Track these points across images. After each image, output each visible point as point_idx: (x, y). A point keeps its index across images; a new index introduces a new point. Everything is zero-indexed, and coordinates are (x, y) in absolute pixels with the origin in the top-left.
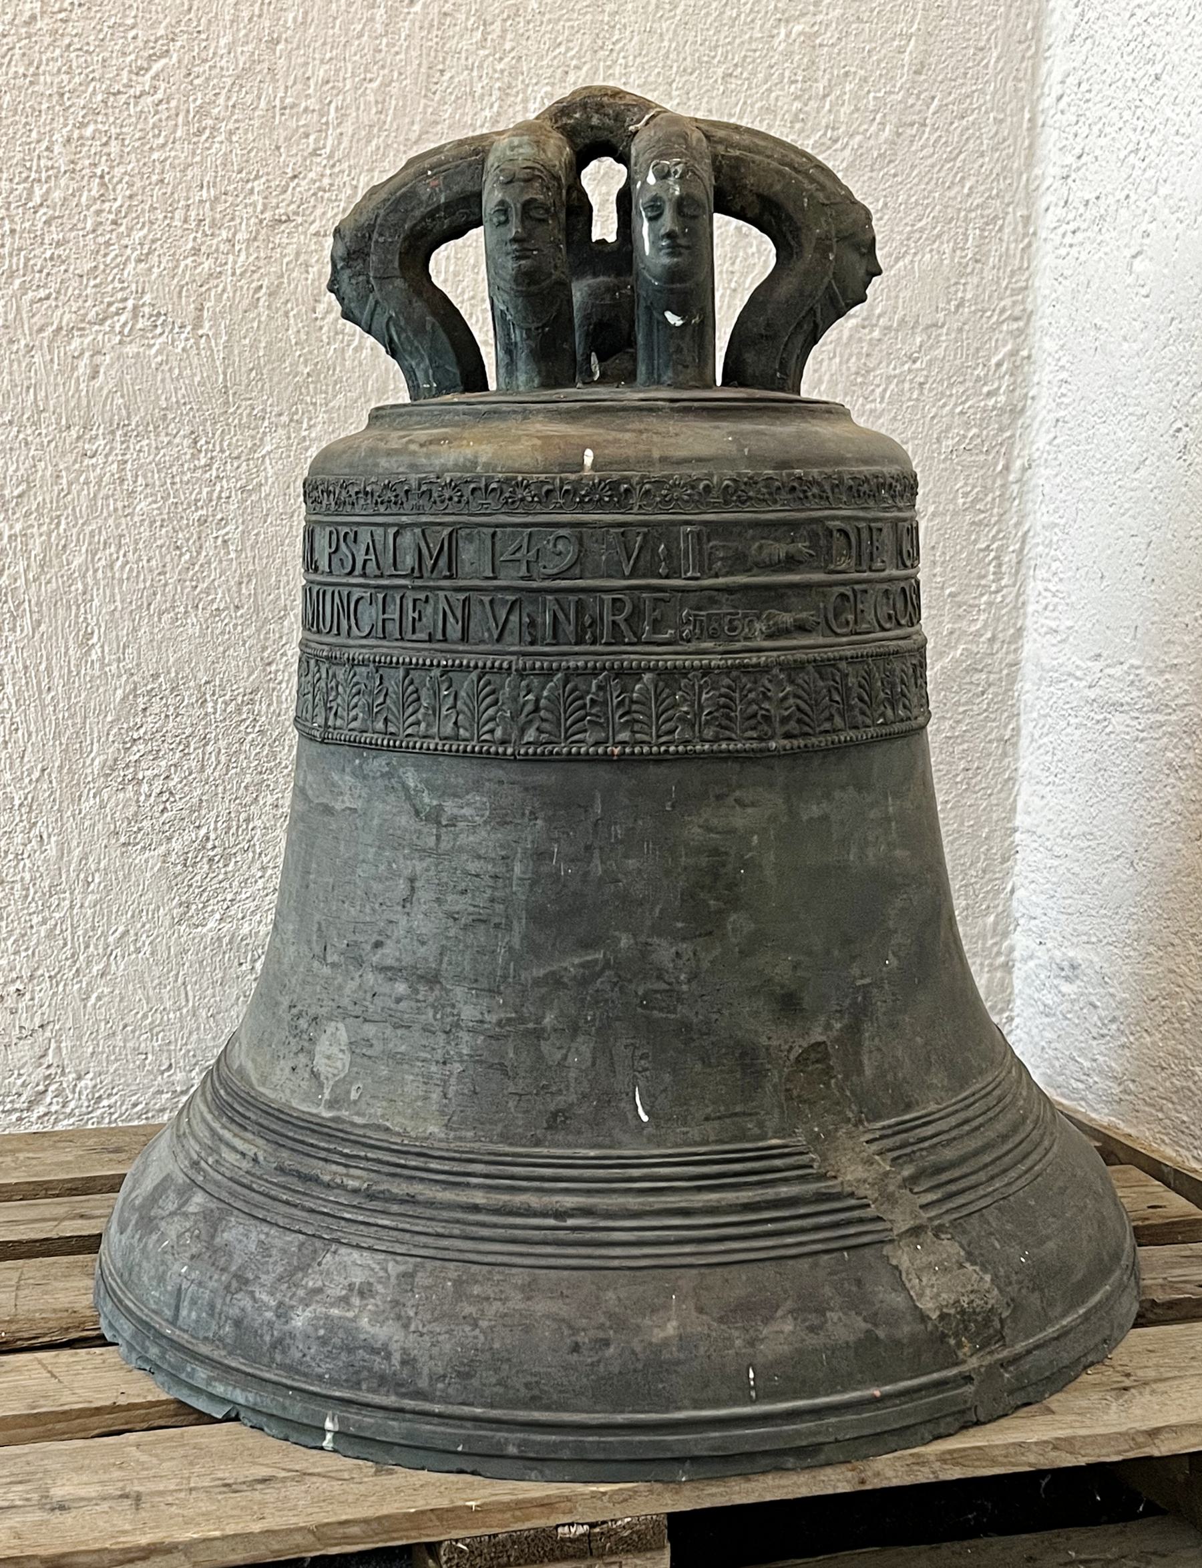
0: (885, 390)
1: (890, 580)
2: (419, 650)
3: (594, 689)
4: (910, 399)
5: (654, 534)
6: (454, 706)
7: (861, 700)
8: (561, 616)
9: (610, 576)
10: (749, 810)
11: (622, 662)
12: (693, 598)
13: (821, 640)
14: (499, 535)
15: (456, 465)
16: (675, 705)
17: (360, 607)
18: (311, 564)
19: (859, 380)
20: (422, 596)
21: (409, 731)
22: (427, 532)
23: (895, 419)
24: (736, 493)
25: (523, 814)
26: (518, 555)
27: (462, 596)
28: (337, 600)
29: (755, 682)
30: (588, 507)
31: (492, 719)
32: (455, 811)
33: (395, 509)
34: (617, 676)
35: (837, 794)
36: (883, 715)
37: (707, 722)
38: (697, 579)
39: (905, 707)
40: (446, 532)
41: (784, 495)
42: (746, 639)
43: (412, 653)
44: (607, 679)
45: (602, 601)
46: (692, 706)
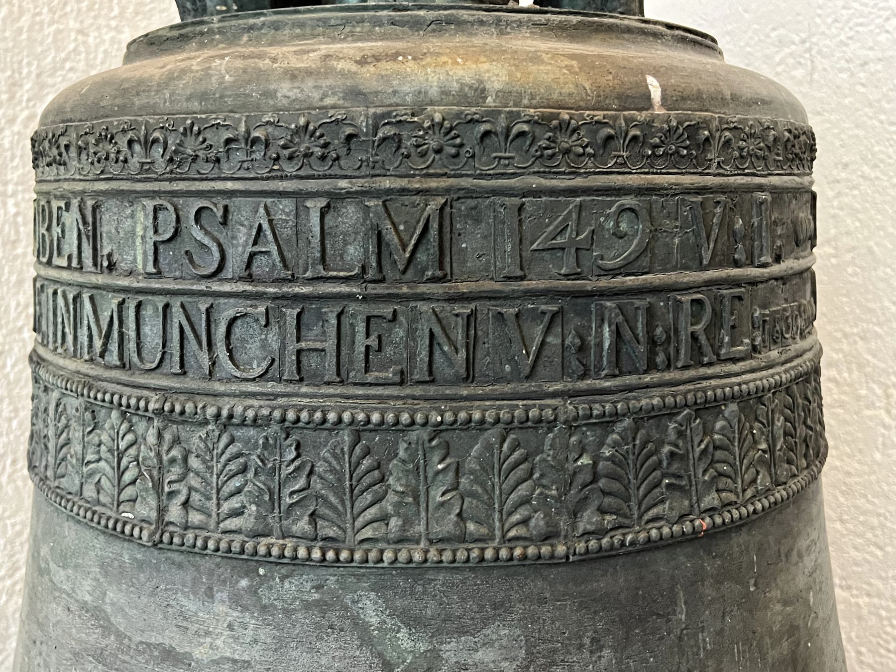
2: (381, 398)
3: (672, 436)
6: (455, 487)
8: (627, 334)
9: (686, 268)
11: (704, 390)
14: (528, 208)
15: (445, 93)
17: (237, 331)
18: (46, 251)
20: (387, 310)
21: (368, 533)
22: (392, 206)
25: (581, 646)
26: (559, 240)
27: (465, 309)
28: (61, 302)
30: (660, 164)
31: (525, 501)
32: (463, 657)
33: (321, 169)
40: (435, 204)
43: (373, 403)
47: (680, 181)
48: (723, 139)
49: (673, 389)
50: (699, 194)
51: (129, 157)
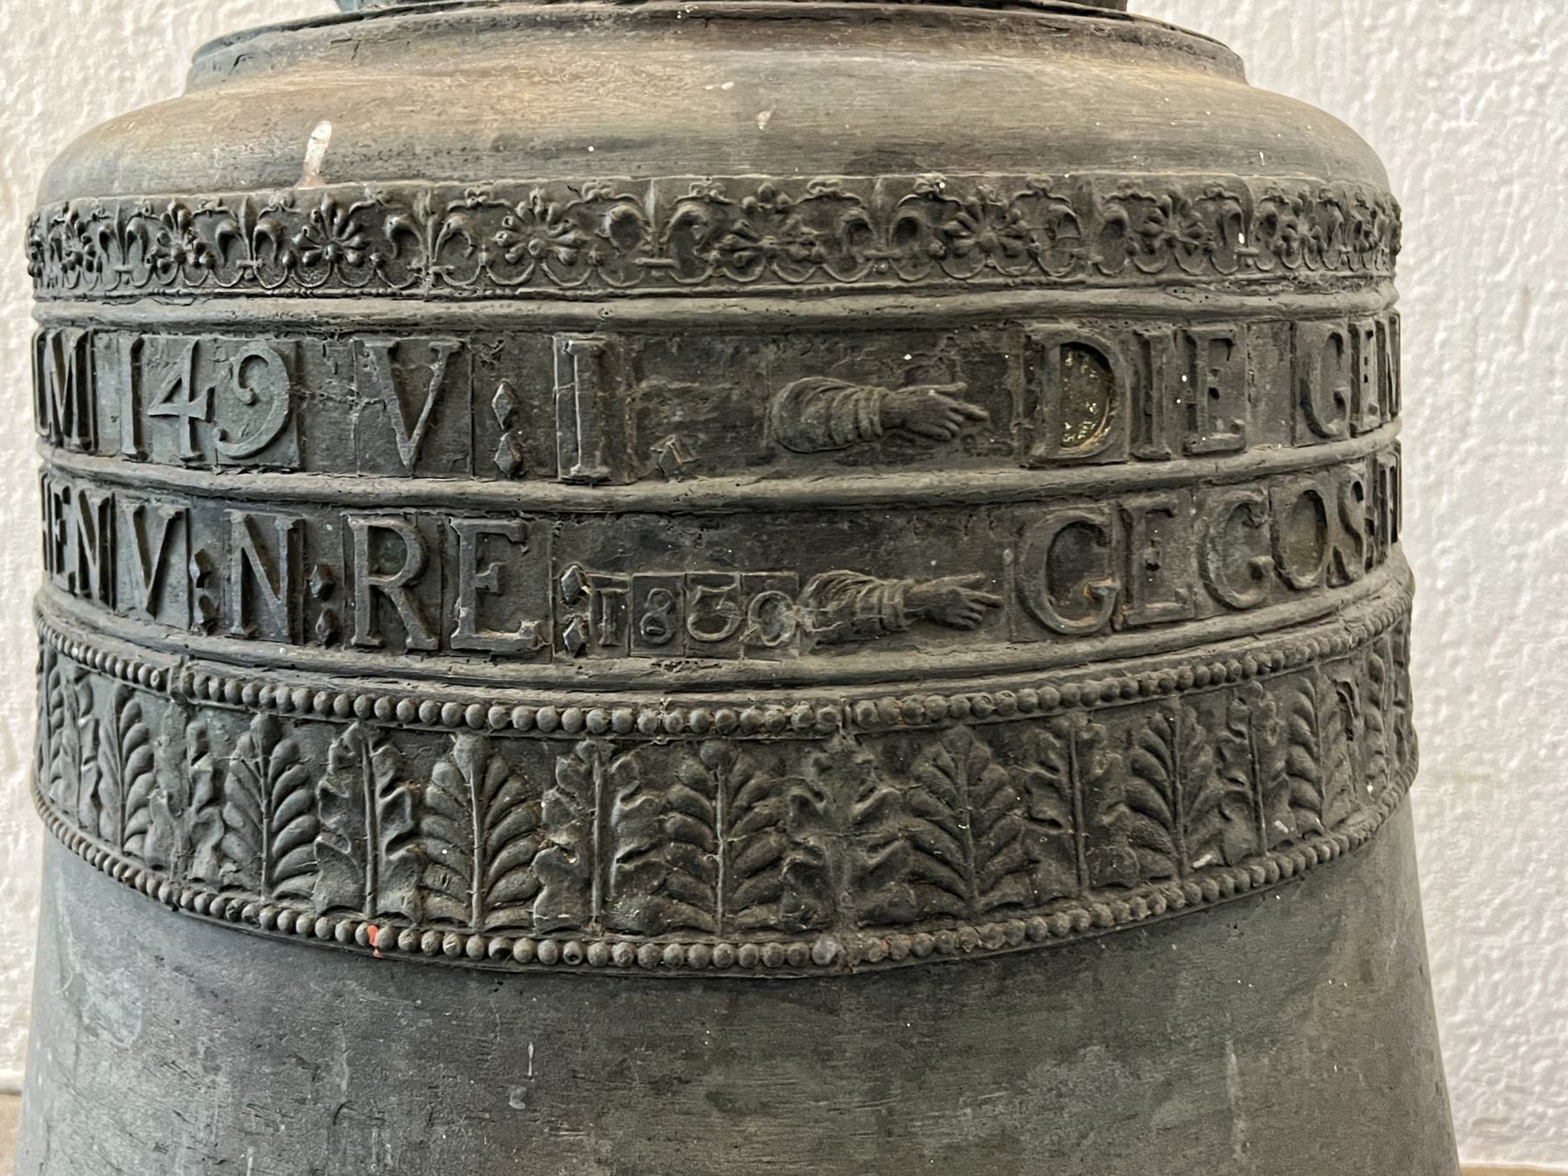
0: (1476, 100)
1: (1264, 475)
4: (1519, 112)
5: (473, 351)
7: (1139, 807)
8: (259, 569)
10: (752, 1126)
12: (594, 533)
13: (1001, 652)
16: (533, 828)
19: (1432, 83)
23: (1491, 144)
24: (721, 236)
25: (194, 1053)
29: (781, 769)
30: (315, 277)
34: (385, 736)
35: (1047, 1071)
36: (1216, 840)
37: (625, 878)
38: (601, 482)
39: (1296, 803)
41: (879, 245)
42: (754, 649)
44: (358, 742)
45: (348, 532)
46: (583, 832)
47: (339, 311)
48: (445, 229)
49: (337, 681)
50: (392, 333)
51: (104, 260)
